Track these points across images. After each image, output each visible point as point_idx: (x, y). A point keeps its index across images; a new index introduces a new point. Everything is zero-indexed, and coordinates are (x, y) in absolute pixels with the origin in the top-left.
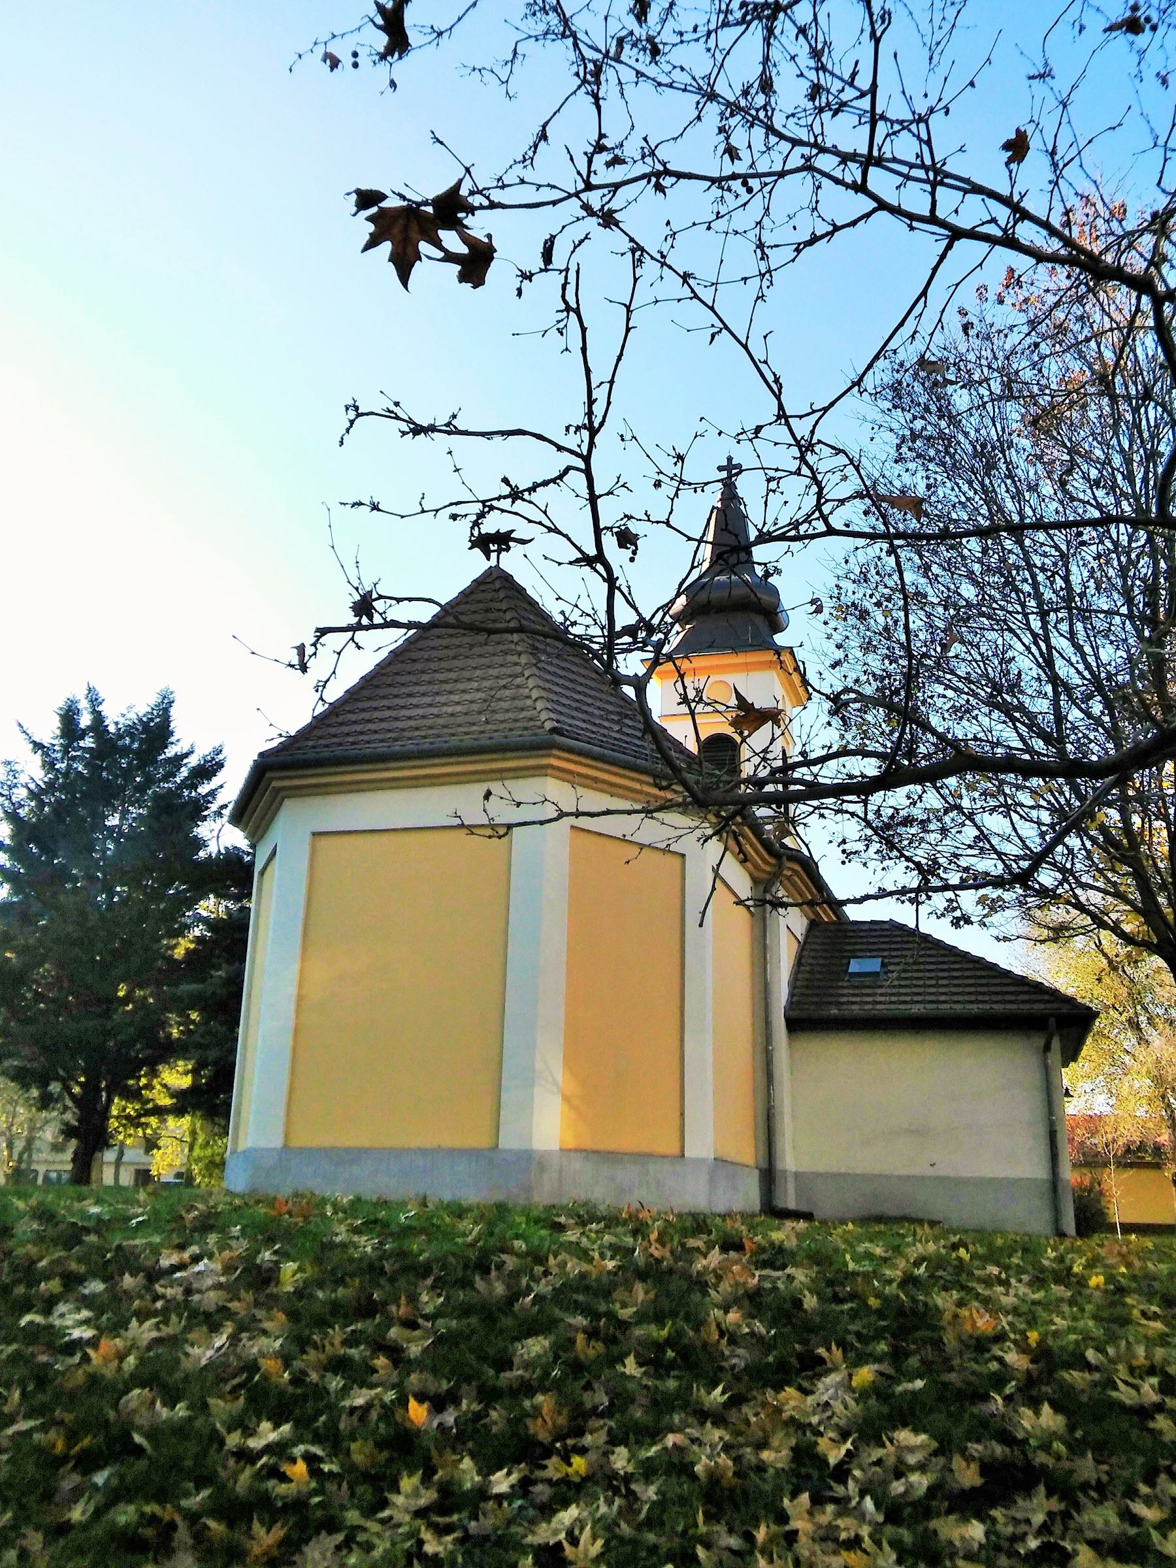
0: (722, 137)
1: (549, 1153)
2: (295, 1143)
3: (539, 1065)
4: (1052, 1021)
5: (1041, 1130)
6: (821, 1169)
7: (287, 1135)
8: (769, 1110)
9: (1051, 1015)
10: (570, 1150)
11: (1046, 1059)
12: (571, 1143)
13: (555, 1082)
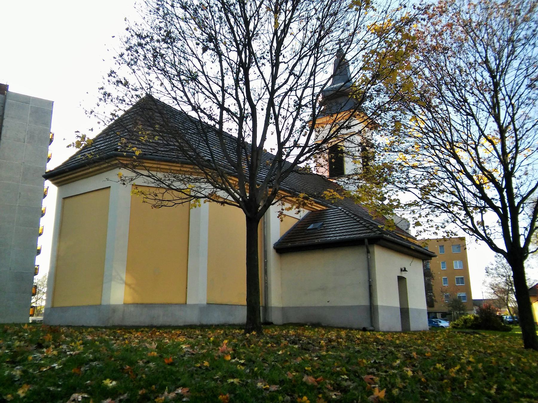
0: (120, 85)
1: (119, 305)
2: (57, 305)
3: (114, 274)
4: (366, 241)
5: (367, 285)
6: (291, 306)
7: (53, 302)
8: (370, 282)
9: (366, 238)
10: (129, 304)
11: (368, 256)
12: (130, 300)
13: (122, 279)
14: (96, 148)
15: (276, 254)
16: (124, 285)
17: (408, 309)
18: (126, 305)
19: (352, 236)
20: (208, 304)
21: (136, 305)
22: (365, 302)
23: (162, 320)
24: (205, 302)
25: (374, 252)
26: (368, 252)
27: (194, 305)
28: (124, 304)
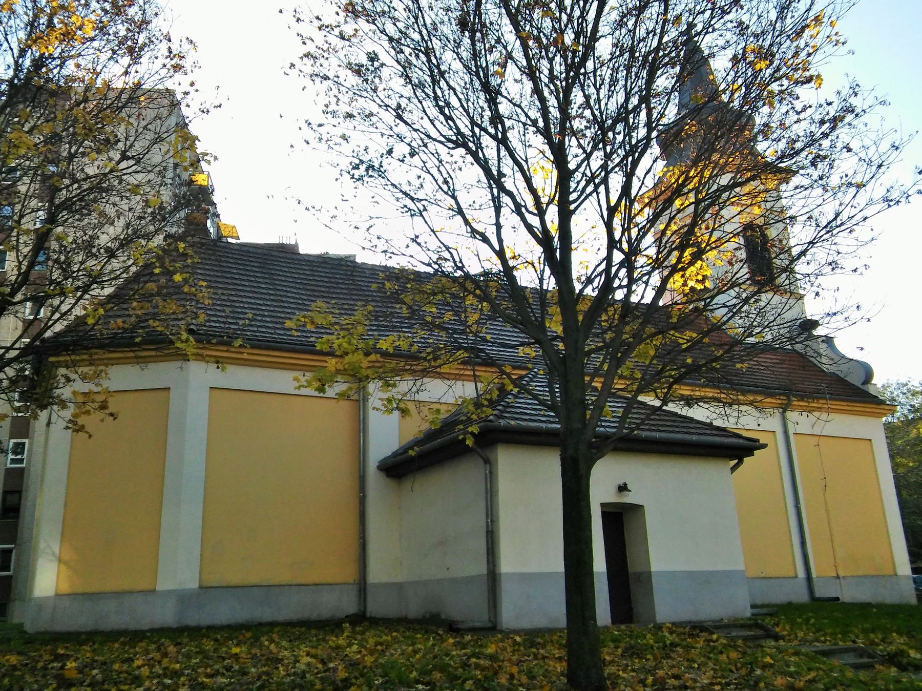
10: (63, 595)
12: (65, 588)
14: (353, 280)
15: (388, 480)
16: (55, 565)
17: (649, 574)
18: (58, 596)
19: (531, 424)
20: (201, 587)
21: (73, 596)
22: (481, 568)
23: (266, 614)
24: (193, 584)
25: (497, 460)
26: (487, 461)
27: (169, 593)
28: (57, 595)
